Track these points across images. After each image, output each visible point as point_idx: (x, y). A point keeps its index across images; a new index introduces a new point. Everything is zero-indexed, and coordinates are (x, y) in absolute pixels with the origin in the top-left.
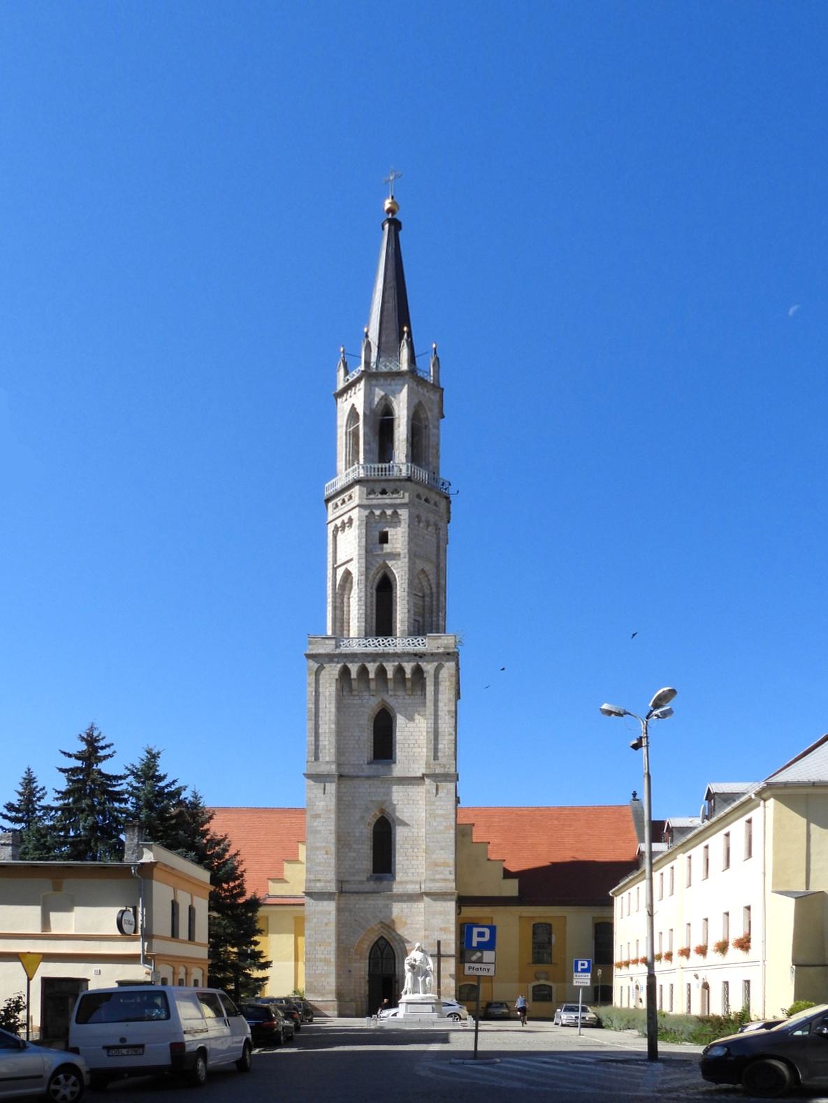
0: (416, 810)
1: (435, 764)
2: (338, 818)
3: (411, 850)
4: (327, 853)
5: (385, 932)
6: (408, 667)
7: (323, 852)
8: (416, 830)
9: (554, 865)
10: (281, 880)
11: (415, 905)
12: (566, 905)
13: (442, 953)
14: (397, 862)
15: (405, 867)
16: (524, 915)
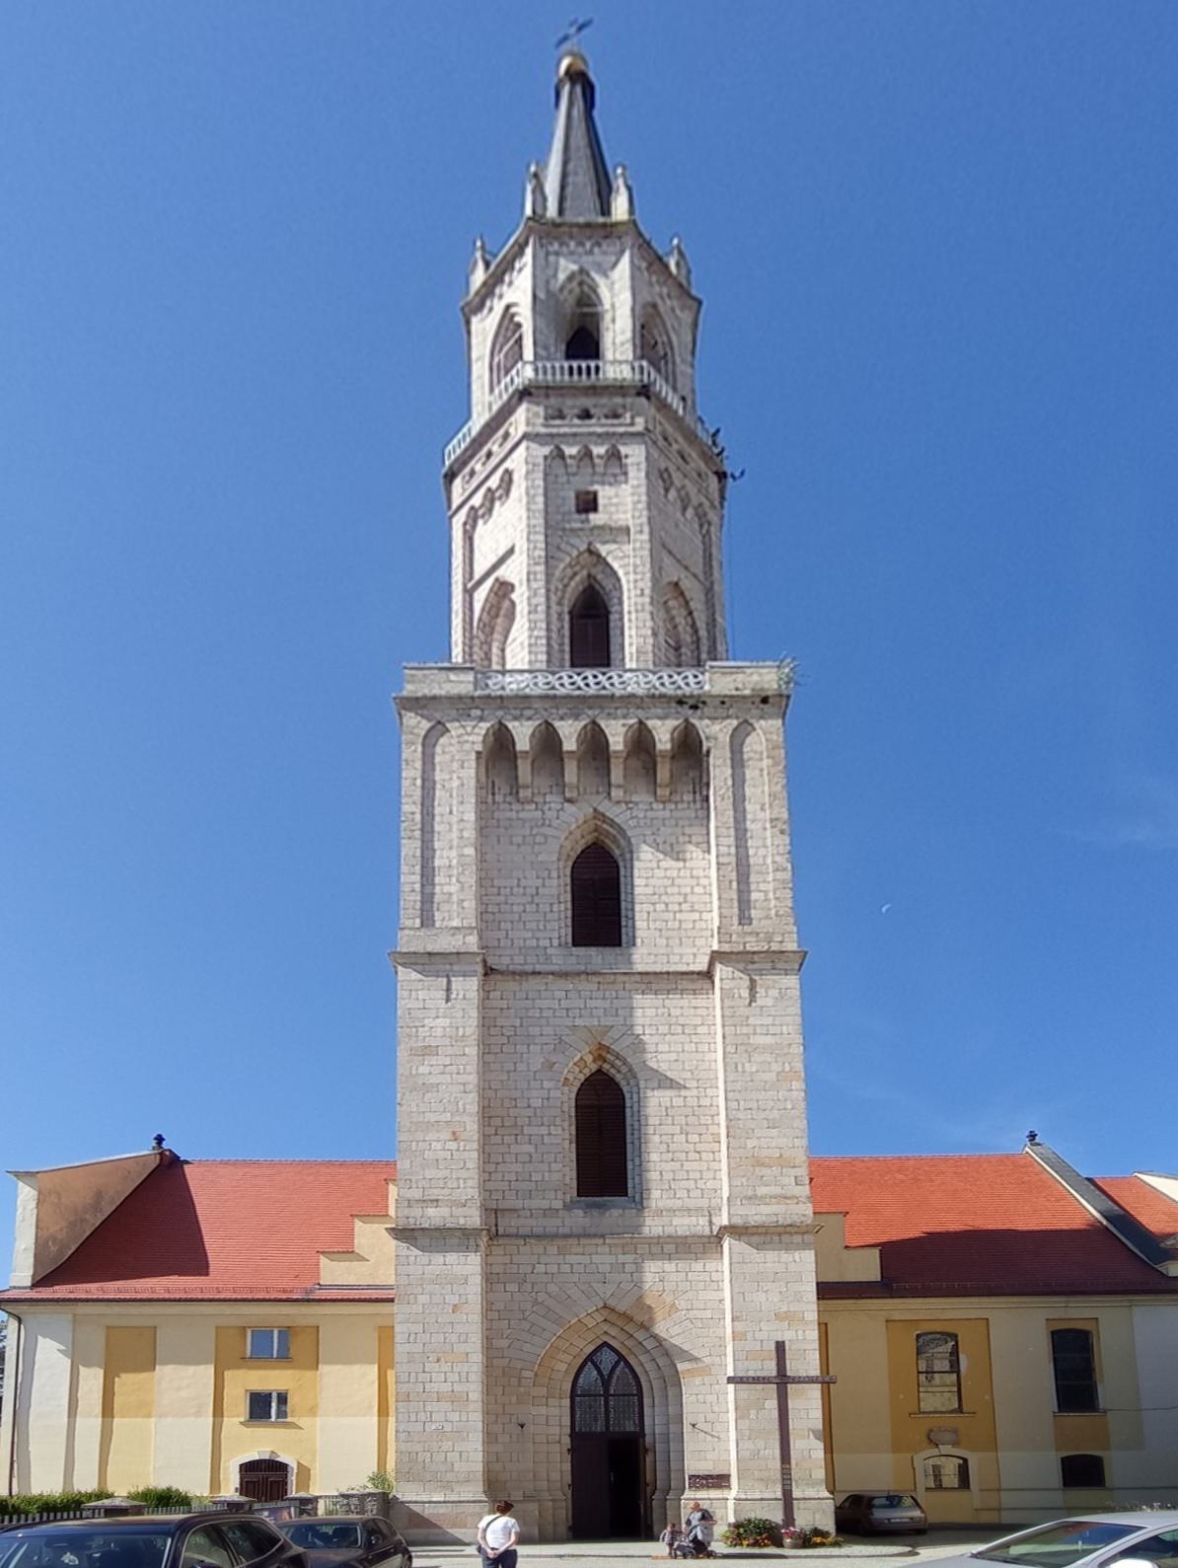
2: (485, 1068)
5: (613, 1332)
6: (663, 732)
7: (446, 1135)
8: (695, 1092)
9: (932, 1236)
10: (348, 1253)
15: (668, 1176)
16: (897, 1316)
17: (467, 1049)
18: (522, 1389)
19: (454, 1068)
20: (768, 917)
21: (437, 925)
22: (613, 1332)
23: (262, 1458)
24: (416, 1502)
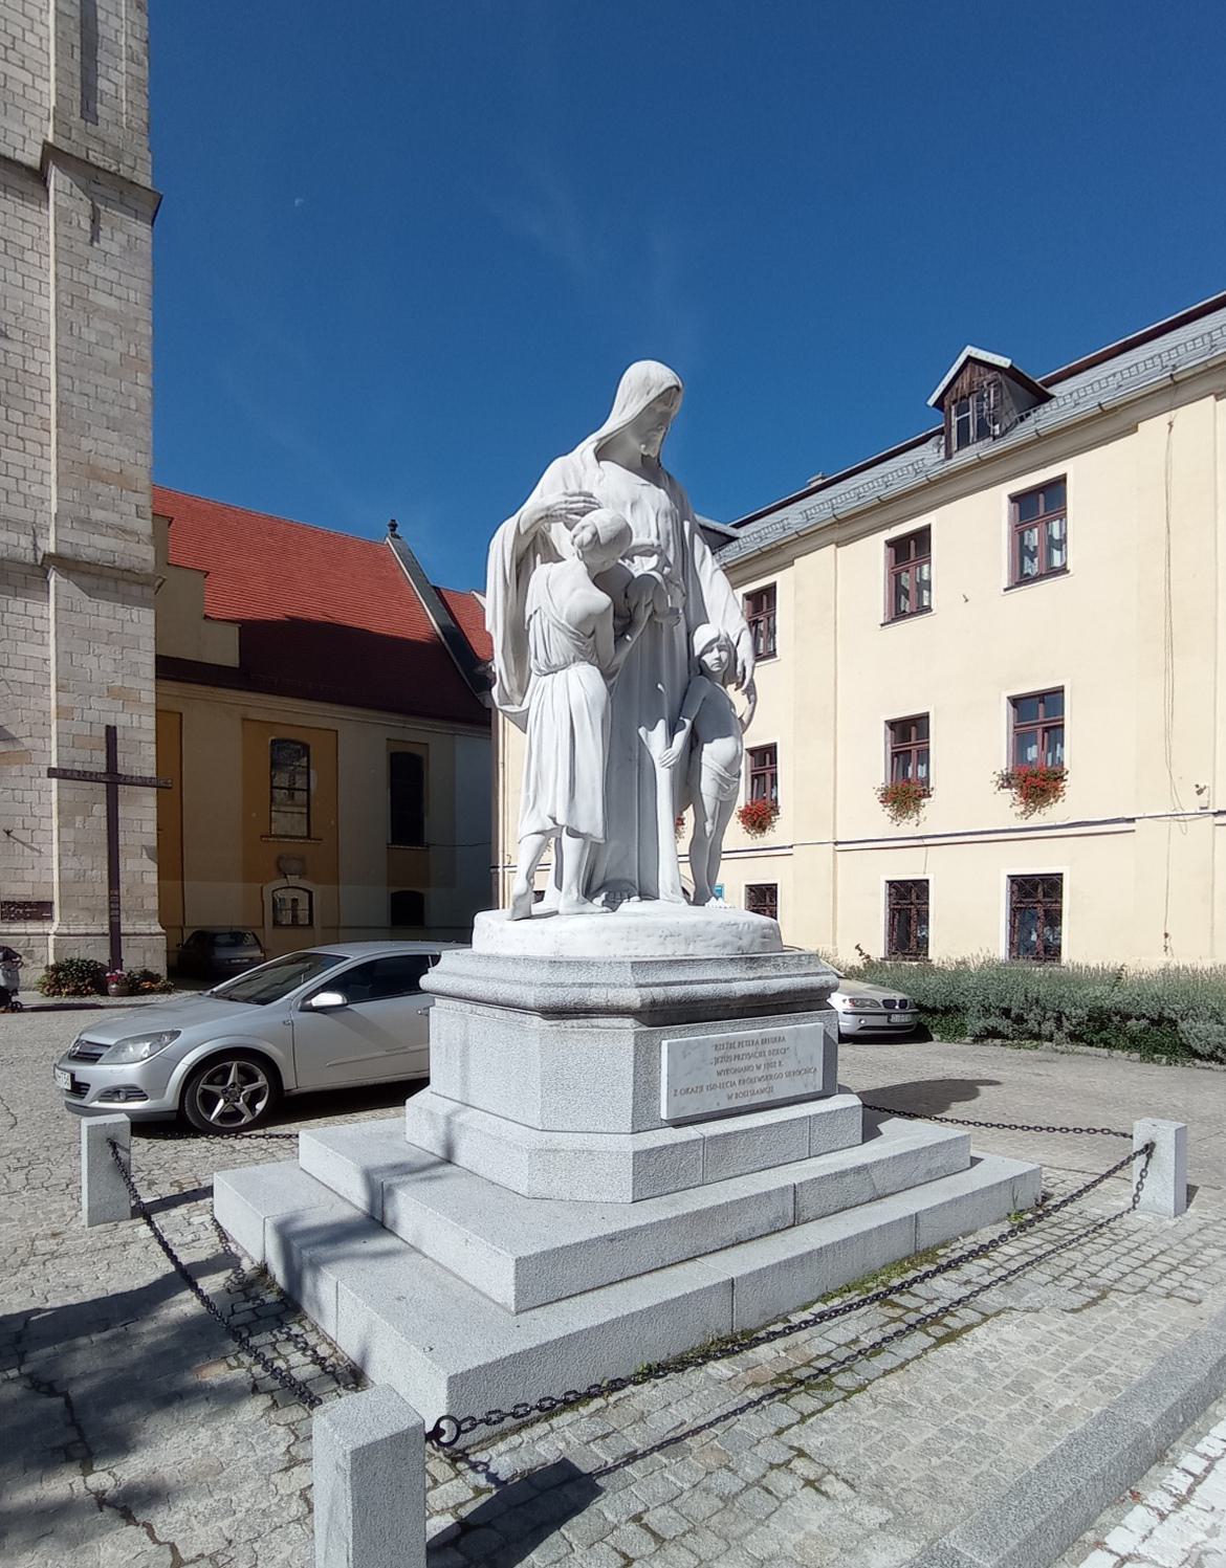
12: (340, 702)
20: (117, 124)
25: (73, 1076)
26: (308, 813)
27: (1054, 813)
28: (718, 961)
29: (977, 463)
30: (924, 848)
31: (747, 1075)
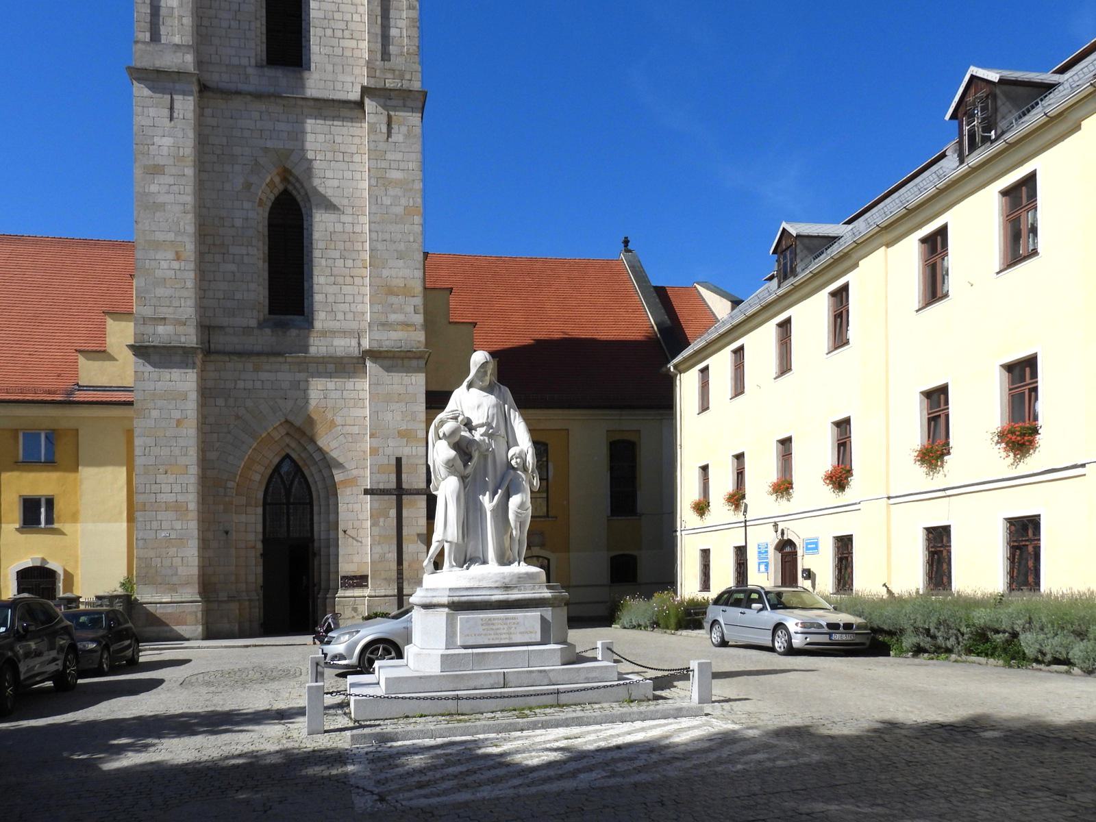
0: (348, 175)
1: (384, 70)
2: (201, 186)
3: (340, 263)
4: (178, 258)
5: (293, 445)
7: (171, 255)
11: (350, 384)
13: (405, 486)
14: (316, 288)
15: (331, 299)
17: (186, 170)
18: (227, 499)
19: (175, 188)
20: (402, 54)
21: (163, 42)
22: (293, 445)
23: (35, 565)
24: (151, 603)
25: (323, 650)
26: (547, 497)
27: (1033, 462)
28: (490, 588)
29: (937, 193)
30: (948, 498)
31: (498, 632)
